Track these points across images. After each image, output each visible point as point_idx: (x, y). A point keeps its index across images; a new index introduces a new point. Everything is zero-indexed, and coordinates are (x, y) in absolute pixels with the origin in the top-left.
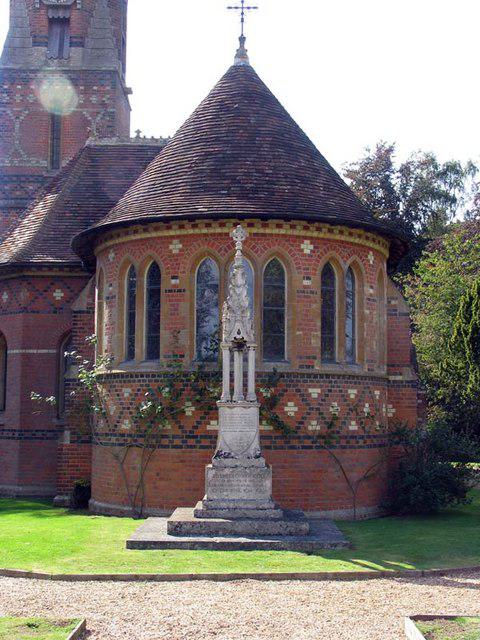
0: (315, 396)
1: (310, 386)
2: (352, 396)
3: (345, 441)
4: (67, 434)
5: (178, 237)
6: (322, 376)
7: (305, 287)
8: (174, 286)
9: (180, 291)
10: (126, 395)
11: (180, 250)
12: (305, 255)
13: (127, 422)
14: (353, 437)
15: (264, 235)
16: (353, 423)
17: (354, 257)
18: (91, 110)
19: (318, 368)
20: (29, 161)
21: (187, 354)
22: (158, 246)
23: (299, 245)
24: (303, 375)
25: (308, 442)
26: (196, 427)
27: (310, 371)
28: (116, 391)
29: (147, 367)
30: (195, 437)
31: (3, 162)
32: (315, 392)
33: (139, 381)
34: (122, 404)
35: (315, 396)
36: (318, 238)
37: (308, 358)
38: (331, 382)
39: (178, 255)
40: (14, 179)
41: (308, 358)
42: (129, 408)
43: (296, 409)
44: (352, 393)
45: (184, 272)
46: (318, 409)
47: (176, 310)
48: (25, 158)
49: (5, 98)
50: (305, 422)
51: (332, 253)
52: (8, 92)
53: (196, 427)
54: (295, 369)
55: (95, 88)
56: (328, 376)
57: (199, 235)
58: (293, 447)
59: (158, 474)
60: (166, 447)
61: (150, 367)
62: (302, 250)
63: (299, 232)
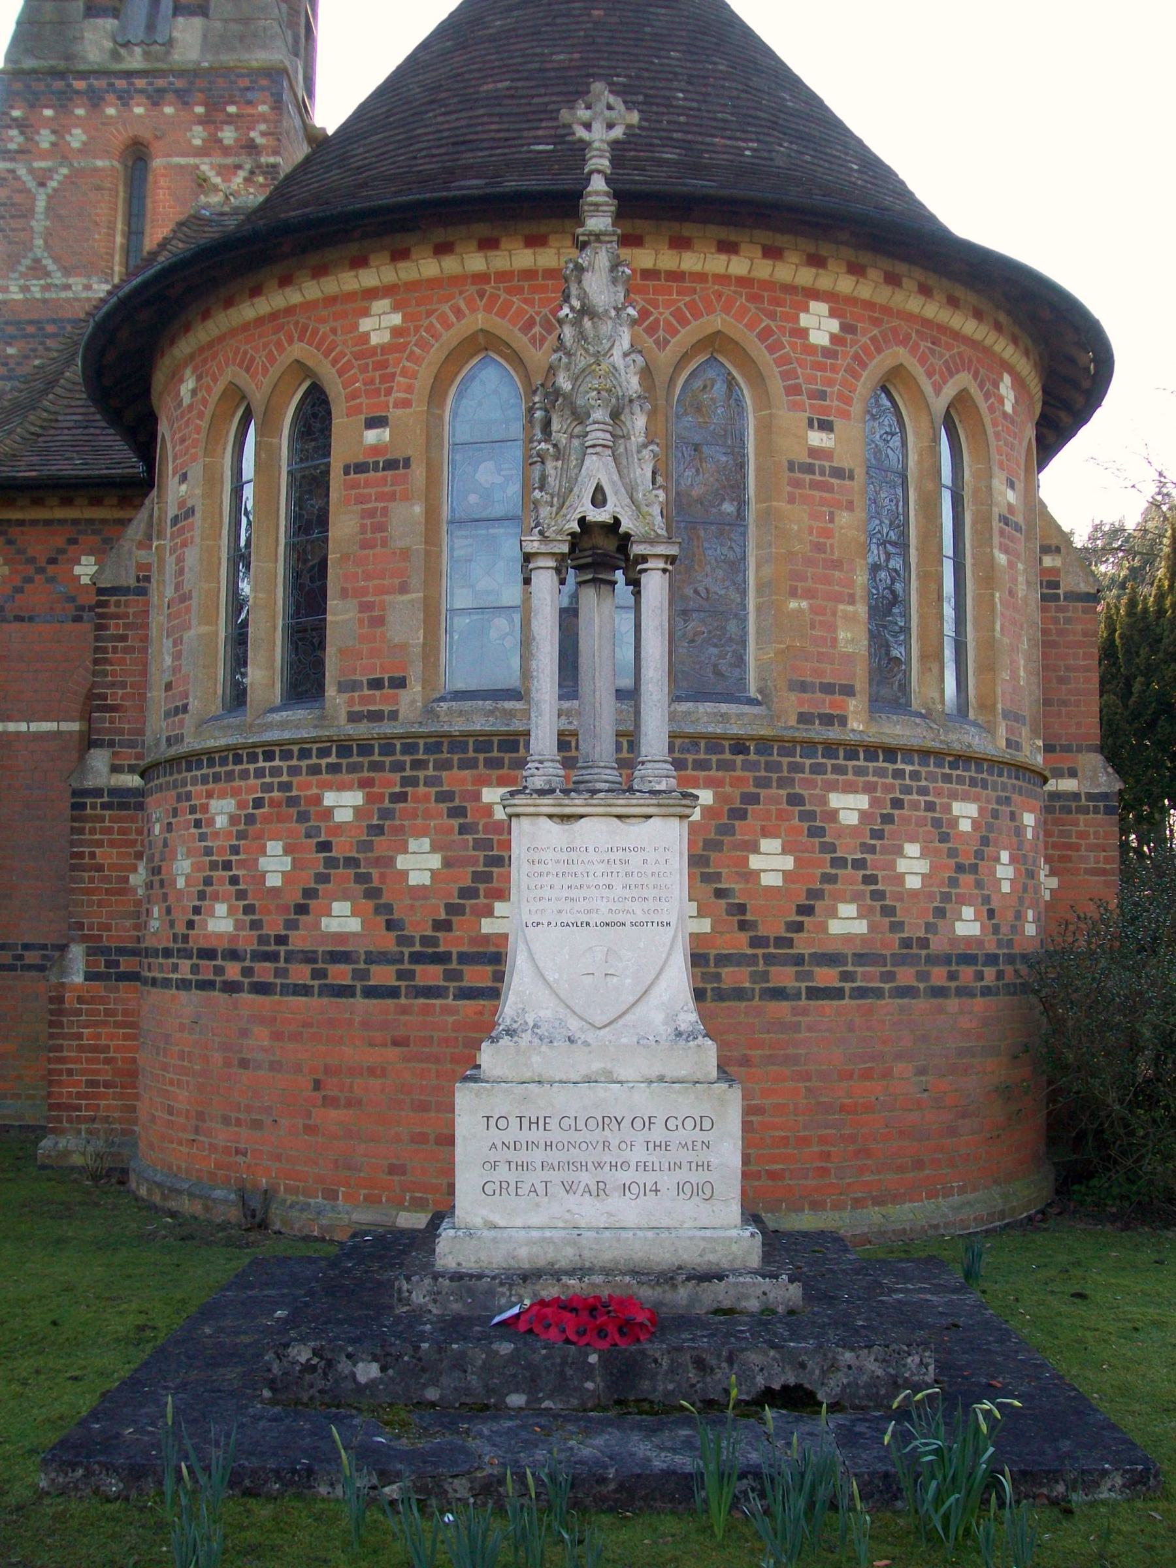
0: (850, 819)
1: (833, 787)
2: (965, 826)
3: (307, 969)
4: (77, 952)
5: (387, 291)
6: (871, 751)
7: (814, 452)
8: (376, 449)
9: (391, 465)
10: (221, 822)
11: (396, 332)
12: (811, 349)
13: (221, 909)
14: (968, 959)
15: (676, 276)
16: (968, 912)
17: (963, 379)
18: (219, 160)
19: (858, 723)
20: (68, 287)
21: (414, 675)
22: (324, 329)
23: (796, 319)
24: (809, 747)
25: (826, 976)
26: (443, 926)
27: (833, 733)
28: (193, 810)
29: (283, 725)
30: (441, 958)
31: (5, 290)
32: (850, 807)
33: (260, 773)
34: (208, 851)
35: (850, 819)
36: (851, 300)
37: (828, 689)
38: (898, 774)
39: (385, 349)
40: (31, 329)
41: (828, 689)
42: (227, 866)
43: (788, 863)
44: (965, 813)
45: (406, 403)
46: (859, 864)
47: (380, 528)
48: (58, 278)
49: (15, 138)
50: (819, 905)
51: (900, 354)
52: (22, 125)
53: (443, 926)
54: (787, 724)
55: (232, 109)
56: (891, 753)
57: (456, 281)
58: (778, 994)
59: (317, 1085)
60: (345, 991)
61: (297, 724)
62: (804, 333)
63: (791, 271)
